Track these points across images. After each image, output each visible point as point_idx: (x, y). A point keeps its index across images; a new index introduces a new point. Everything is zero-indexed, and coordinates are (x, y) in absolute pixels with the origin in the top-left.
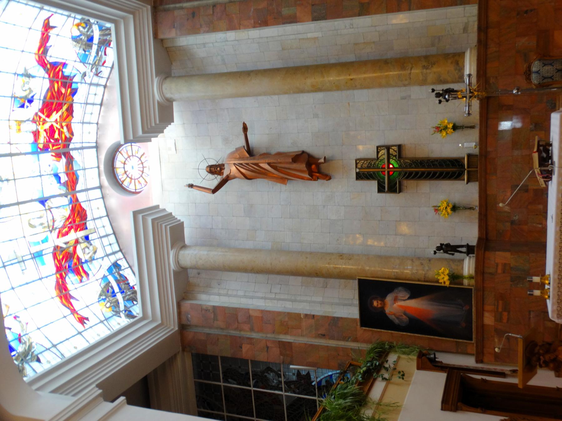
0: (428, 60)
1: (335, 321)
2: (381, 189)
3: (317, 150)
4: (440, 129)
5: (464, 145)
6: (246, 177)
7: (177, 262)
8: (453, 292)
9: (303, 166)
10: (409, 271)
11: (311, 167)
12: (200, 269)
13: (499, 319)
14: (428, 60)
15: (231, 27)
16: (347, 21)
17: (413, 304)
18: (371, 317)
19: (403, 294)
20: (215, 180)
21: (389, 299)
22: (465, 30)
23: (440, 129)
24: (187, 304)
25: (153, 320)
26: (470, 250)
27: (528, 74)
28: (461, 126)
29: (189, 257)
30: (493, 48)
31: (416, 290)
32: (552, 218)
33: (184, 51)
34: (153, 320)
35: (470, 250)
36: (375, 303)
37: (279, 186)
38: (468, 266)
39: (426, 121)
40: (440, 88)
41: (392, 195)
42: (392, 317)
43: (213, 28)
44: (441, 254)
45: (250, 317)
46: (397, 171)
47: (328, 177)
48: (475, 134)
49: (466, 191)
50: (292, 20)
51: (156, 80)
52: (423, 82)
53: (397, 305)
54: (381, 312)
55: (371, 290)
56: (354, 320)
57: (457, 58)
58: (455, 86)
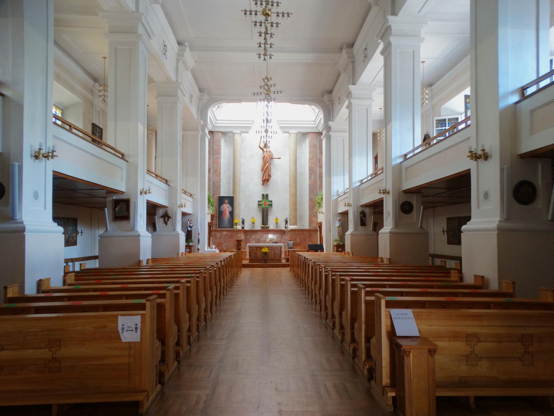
0: (295, 217)
1: (219, 187)
2: (259, 201)
3: (271, 180)
4: (277, 219)
5: (271, 225)
6: (264, 158)
7: (236, 133)
8: (232, 223)
9: (267, 178)
10: (236, 212)
11: (266, 181)
12: (234, 140)
13: (225, 235)
14: (295, 217)
15: (310, 159)
16: (308, 194)
17: (227, 213)
18: (221, 200)
19: (230, 209)
20: (262, 146)
21: (229, 205)
22: (303, 225)
23: (277, 219)
24: (220, 134)
25: (216, 123)
26: (243, 228)
27: (290, 240)
28: (265, 164)
29: (237, 137)
30: (297, 233)
31: (232, 213)
32: (141, 215)
33: (304, 141)
34: (216, 123)
35: (243, 228)
36: (226, 201)
37: (260, 168)
38: (239, 227)
39: (279, 216)
40: (288, 220)
41: (257, 204)
42: (222, 206)
43: (310, 153)
44: (241, 220)
45: (218, 159)
46: (265, 208)
47: (263, 185)
48: (275, 228)
49: (258, 226)
50: (310, 178)
51: (296, 132)
52: (290, 215)
53: (226, 207)
54: (223, 203)
55: (231, 200)
56: (220, 194)
57: (295, 224)
58: (288, 224)
